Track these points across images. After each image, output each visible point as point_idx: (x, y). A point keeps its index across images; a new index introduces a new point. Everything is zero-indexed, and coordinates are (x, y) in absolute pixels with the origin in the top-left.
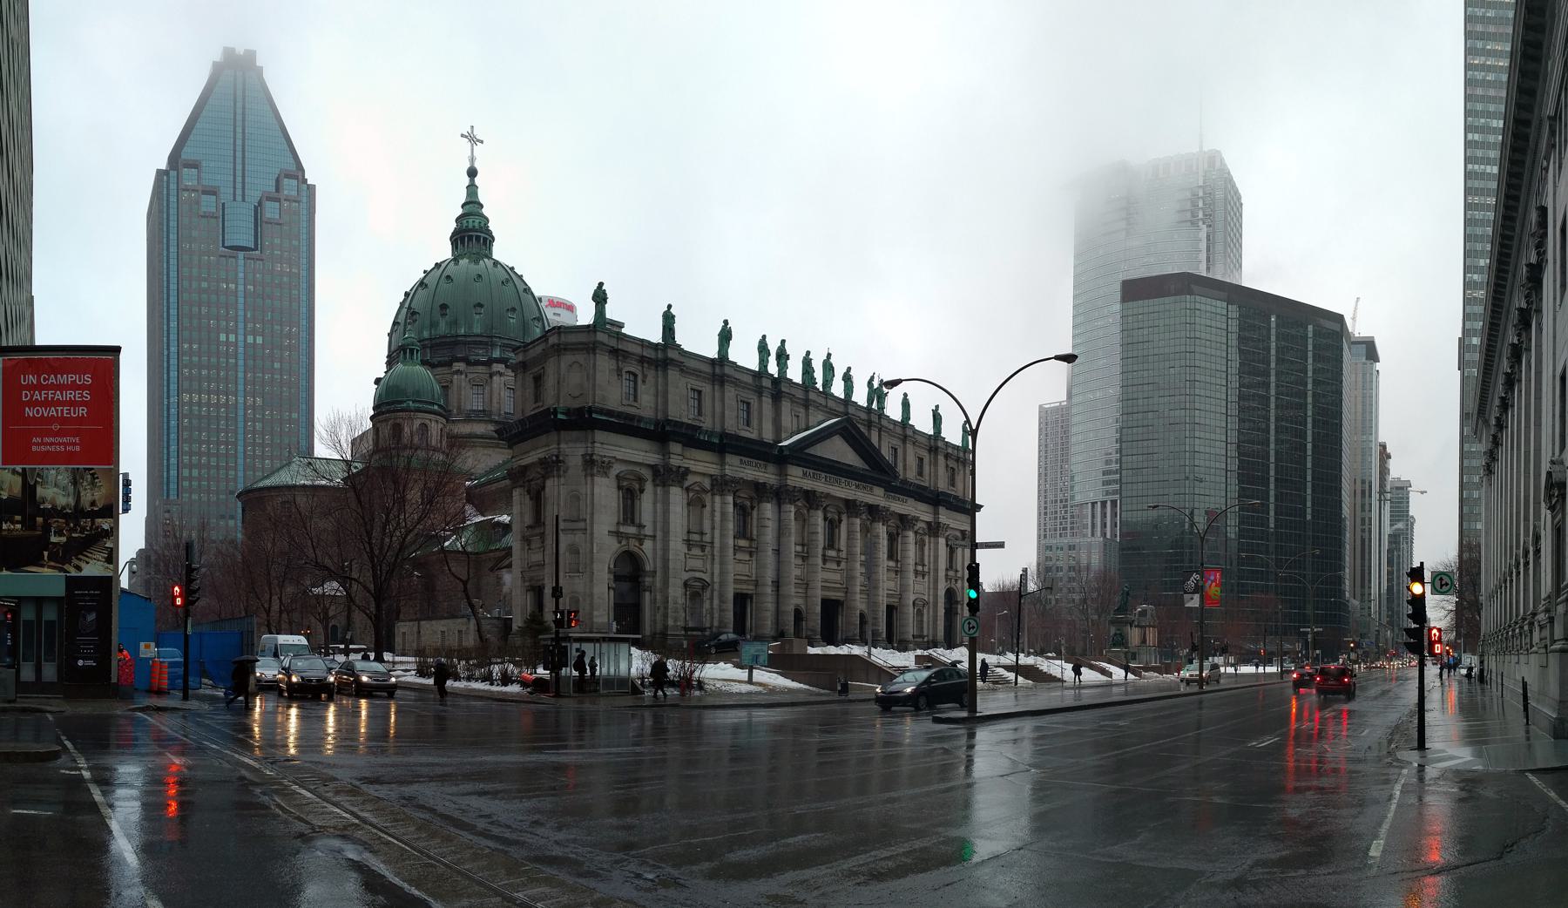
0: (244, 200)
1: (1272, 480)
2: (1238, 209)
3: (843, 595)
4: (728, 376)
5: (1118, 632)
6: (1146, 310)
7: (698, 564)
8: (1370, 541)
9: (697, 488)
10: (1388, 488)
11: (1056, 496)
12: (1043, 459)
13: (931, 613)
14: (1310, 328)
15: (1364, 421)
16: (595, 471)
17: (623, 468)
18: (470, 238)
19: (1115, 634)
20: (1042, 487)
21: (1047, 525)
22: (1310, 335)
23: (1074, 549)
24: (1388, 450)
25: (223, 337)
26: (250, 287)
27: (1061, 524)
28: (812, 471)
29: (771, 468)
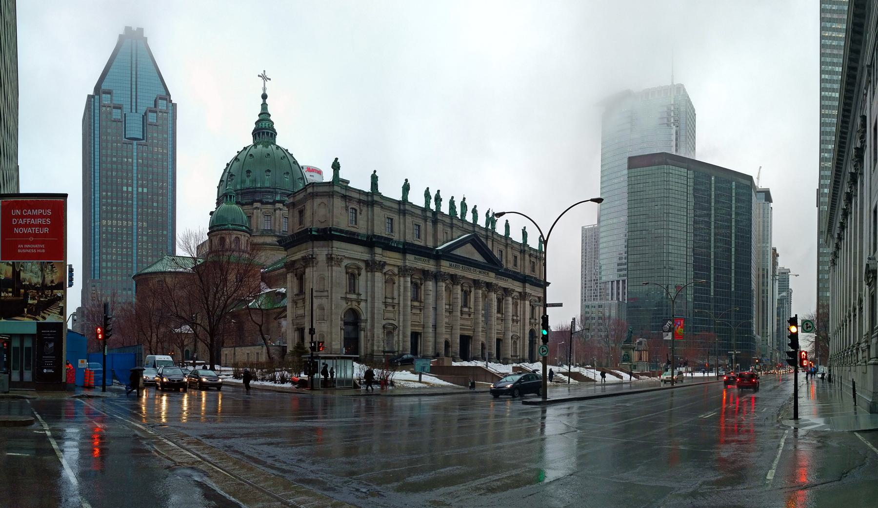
0: (136, 112)
3: (472, 333)
4: (408, 210)
7: (391, 315)
9: (390, 273)
10: (777, 273)
12: (584, 257)
13: (521, 343)
14: (734, 183)
16: (333, 263)
17: (349, 262)
18: (263, 133)
19: (625, 355)
24: (777, 252)
25: (125, 189)
26: (140, 161)
27: (594, 293)
28: (455, 264)
29: (432, 262)
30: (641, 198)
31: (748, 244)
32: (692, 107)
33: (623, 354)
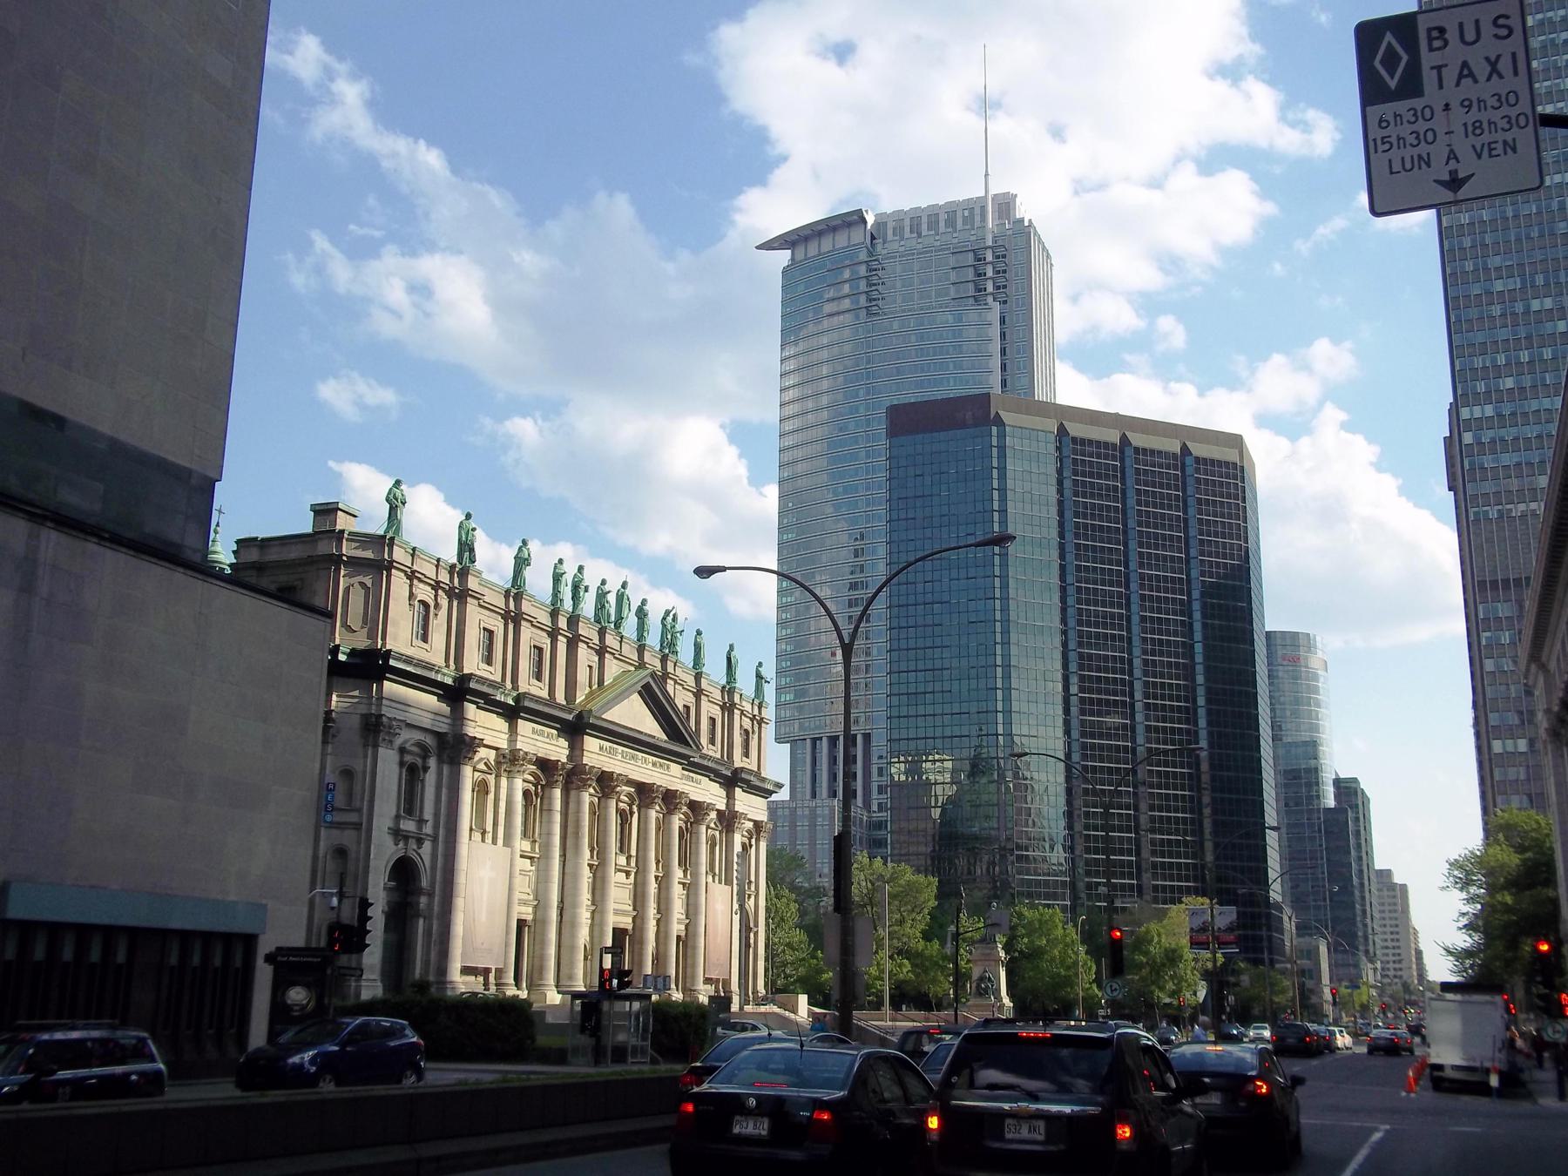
22: (1228, 752)
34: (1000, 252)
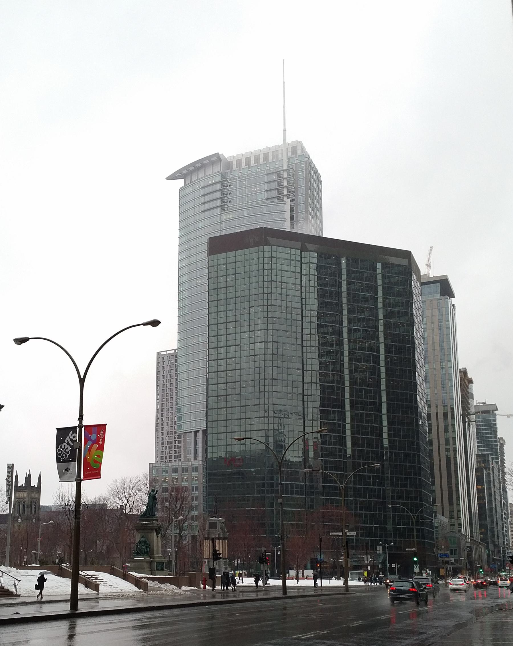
1: (347, 402)
2: (318, 186)
5: (143, 539)
6: (229, 261)
8: (455, 458)
10: (473, 411)
11: (171, 428)
14: (379, 265)
15: (442, 349)
19: (140, 542)
20: (159, 421)
21: (164, 453)
23: (187, 471)
24: (470, 376)
27: (176, 452)
30: (229, 296)
31: (409, 359)
32: (316, 172)
33: (137, 540)
34: (292, 172)
